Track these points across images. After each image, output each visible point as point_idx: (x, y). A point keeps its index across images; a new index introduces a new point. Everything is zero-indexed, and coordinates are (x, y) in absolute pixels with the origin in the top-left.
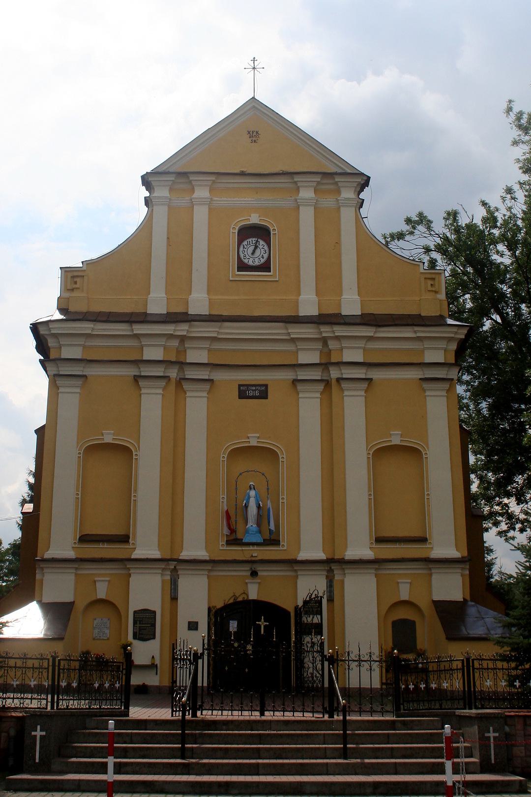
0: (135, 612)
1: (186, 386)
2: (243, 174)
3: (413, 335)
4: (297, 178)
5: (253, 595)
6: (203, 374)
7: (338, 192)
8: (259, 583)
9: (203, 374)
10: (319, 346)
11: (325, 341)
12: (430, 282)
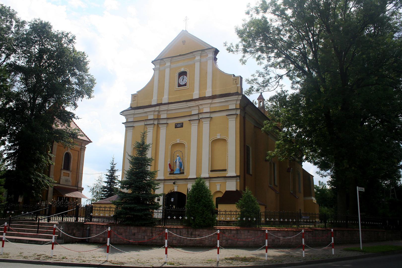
1: (160, 126)
2: (180, 55)
4: (194, 54)
5: (176, 190)
6: (165, 121)
9: (165, 121)
11: (198, 106)
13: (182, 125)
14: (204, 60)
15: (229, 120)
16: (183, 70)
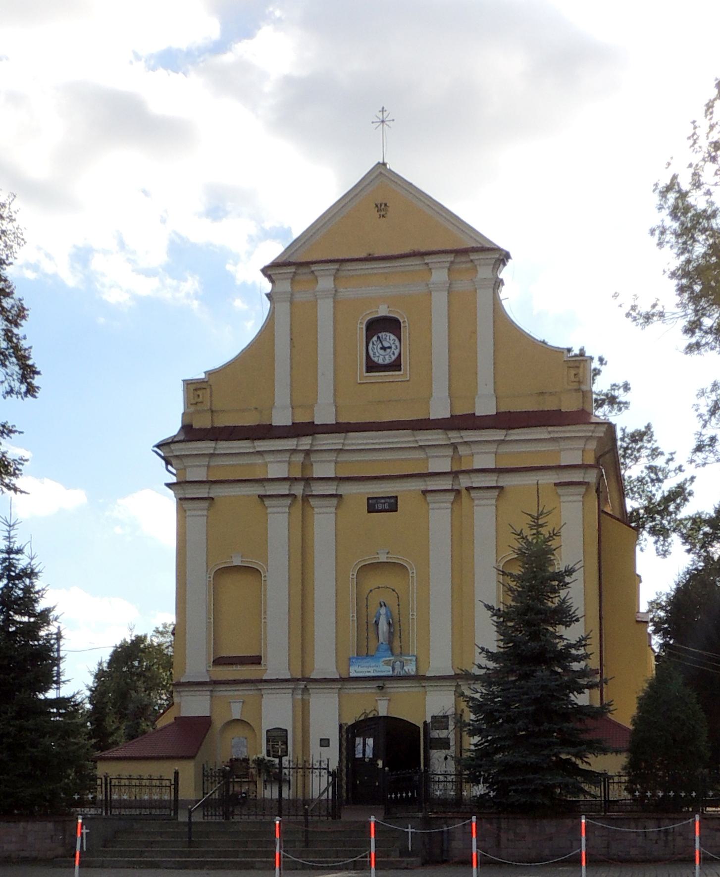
0: (268, 731)
2: (370, 259)
3: (549, 437)
5: (383, 712)
6: (330, 489)
7: (475, 269)
8: (389, 700)
9: (330, 489)
10: (449, 452)
11: (454, 446)
12: (573, 372)
13: (392, 505)
14: (463, 285)
15: (562, 499)
16: (383, 311)
